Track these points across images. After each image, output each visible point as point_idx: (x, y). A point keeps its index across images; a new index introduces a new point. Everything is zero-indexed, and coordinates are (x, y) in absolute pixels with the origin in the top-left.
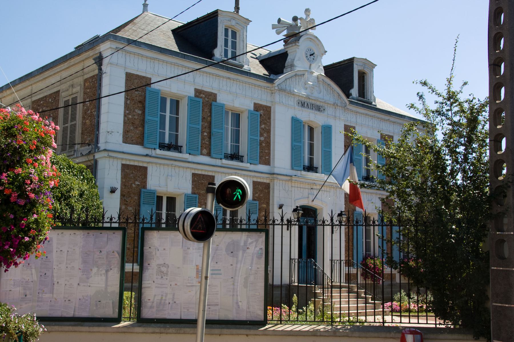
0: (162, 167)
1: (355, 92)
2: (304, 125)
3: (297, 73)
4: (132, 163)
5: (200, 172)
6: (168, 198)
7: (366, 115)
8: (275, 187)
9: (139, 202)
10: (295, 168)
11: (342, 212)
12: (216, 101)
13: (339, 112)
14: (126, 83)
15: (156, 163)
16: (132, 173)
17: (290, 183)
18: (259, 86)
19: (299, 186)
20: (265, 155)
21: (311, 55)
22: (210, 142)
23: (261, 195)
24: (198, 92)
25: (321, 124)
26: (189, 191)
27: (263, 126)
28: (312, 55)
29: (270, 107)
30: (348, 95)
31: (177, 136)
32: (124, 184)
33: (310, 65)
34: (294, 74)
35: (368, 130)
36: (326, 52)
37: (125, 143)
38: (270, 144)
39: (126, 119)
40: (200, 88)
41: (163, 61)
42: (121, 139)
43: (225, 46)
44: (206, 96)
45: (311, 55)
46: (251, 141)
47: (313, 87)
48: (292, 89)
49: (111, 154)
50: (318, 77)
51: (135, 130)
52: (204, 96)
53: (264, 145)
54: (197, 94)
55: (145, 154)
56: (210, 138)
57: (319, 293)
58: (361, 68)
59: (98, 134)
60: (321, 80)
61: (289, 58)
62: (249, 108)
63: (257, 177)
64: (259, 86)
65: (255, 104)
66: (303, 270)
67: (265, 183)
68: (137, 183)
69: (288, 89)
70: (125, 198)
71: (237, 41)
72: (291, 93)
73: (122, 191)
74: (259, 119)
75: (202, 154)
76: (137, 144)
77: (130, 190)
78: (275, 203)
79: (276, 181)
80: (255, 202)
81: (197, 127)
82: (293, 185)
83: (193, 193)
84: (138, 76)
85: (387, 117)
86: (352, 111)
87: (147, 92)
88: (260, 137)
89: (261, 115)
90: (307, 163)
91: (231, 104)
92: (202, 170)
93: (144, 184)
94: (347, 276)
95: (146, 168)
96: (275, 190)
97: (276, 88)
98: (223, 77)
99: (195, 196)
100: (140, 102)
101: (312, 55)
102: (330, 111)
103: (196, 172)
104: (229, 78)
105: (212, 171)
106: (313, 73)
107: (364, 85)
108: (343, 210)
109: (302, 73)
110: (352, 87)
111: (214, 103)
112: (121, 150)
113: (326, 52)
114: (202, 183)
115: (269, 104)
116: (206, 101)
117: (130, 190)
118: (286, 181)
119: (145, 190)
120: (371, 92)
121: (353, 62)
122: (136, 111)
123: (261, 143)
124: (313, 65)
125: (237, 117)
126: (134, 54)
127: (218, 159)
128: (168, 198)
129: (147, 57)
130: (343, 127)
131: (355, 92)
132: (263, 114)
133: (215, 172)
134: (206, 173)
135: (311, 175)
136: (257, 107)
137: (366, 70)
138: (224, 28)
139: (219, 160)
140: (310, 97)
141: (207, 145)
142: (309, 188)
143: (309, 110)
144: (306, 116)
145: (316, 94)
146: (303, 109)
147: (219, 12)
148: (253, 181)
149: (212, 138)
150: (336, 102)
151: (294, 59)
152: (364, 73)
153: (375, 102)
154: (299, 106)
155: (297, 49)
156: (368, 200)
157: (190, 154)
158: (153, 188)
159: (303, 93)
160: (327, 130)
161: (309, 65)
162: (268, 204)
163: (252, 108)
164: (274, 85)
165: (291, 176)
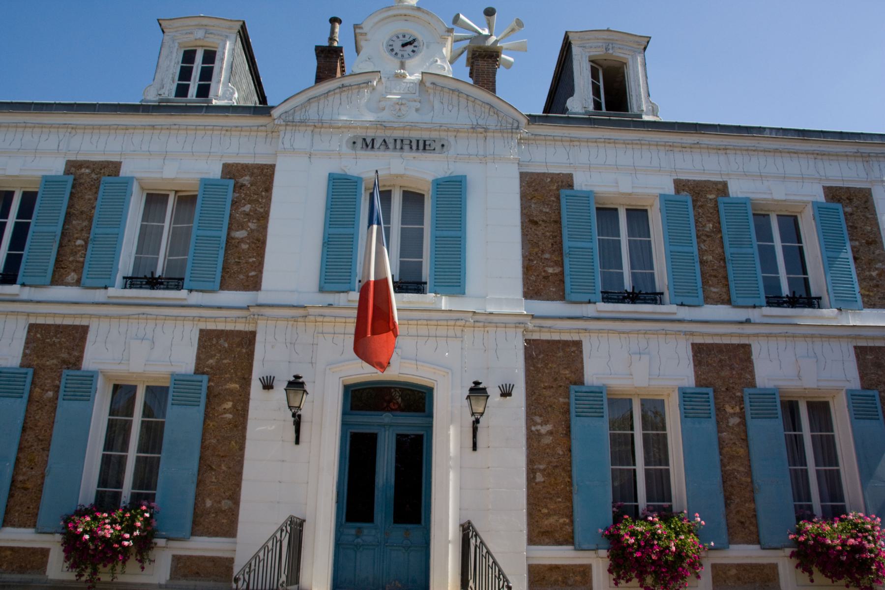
0: (124, 322)
5: (709, 340)
10: (327, 287)
20: (243, 265)
21: (404, 45)
25: (430, 178)
26: (855, 384)
28: (410, 43)
31: (806, 281)
44: (93, 170)
45: (404, 45)
52: (87, 171)
55: (743, 319)
69: (326, 118)
72: (333, 126)
76: (723, 302)
80: (199, 377)
81: (750, 251)
83: (699, 384)
91: (158, 176)
101: (410, 43)
114: (54, 344)
128: (149, 389)
133: (748, 336)
135: (805, 316)
136: (833, 194)
139: (103, 291)
145: (412, 116)
150: (481, 122)
158: (770, 385)
163: (821, 198)
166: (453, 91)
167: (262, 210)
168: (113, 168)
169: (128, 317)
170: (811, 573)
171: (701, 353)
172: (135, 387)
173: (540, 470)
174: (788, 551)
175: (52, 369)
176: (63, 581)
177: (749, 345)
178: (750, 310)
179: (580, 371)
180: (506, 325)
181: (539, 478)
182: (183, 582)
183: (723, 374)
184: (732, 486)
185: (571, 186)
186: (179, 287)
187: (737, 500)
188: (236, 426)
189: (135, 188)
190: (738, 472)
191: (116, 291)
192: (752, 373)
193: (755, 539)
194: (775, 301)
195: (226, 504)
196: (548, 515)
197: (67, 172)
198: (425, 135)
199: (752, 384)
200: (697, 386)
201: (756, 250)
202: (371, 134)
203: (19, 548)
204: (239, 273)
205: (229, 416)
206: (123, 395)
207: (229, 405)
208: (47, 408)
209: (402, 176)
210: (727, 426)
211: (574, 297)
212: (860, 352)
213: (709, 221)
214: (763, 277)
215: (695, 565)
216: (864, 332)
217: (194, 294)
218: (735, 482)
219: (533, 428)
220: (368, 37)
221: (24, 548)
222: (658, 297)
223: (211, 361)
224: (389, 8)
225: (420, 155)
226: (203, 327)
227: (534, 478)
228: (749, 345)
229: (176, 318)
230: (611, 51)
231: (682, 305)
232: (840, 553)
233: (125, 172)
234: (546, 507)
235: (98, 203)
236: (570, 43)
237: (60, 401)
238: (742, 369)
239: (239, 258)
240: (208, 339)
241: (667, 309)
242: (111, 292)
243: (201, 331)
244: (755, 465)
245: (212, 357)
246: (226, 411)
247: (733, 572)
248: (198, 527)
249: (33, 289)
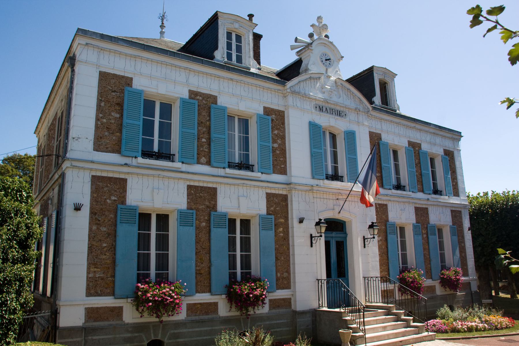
0: (232, 187)
1: (377, 99)
2: (324, 132)
3: (312, 76)
4: (104, 174)
6: (158, 216)
7: (391, 121)
8: (294, 199)
9: (116, 221)
11: (373, 223)
12: (216, 103)
13: (362, 118)
14: (99, 83)
15: (138, 174)
16: (107, 186)
17: (311, 194)
18: (268, 89)
19: (322, 197)
20: (279, 163)
21: (326, 60)
22: (209, 149)
23: (277, 209)
24: (193, 94)
25: (343, 130)
27: (276, 132)
29: (283, 112)
30: (372, 103)
32: (95, 200)
33: (327, 69)
34: (309, 76)
35: (395, 137)
36: (342, 57)
37: (97, 151)
38: (285, 151)
39: (99, 123)
40: (195, 89)
41: (147, 59)
42: (90, 145)
43: (227, 49)
44: (203, 99)
45: (326, 60)
46: (261, 148)
47: (331, 91)
48: (307, 93)
49: (74, 163)
50: (336, 82)
51: (109, 137)
52: (200, 98)
53: (278, 152)
54: (193, 96)
55: (124, 163)
56: (209, 145)
57: (349, 320)
58: (381, 77)
59: (67, 143)
60: (339, 84)
61: (303, 64)
62: (258, 112)
63: (271, 188)
64: (268, 89)
65: (265, 108)
66: (333, 290)
67: (281, 195)
68: (113, 198)
70: (97, 216)
71: (243, 45)
72: (305, 96)
73: (91, 208)
74: (270, 125)
75: (199, 163)
76: (113, 152)
77: (104, 207)
78: (294, 217)
79: (293, 192)
82: (315, 196)
84: (115, 76)
85: (413, 125)
86: (376, 118)
87: (126, 93)
88: (273, 143)
89: (272, 120)
90: (330, 172)
92: (199, 181)
93: (122, 199)
94: (383, 293)
95: (125, 181)
96: (293, 202)
97: (289, 90)
98: (224, 78)
99: (191, 211)
100: (118, 104)
102: (352, 116)
103: (192, 184)
104: (232, 79)
105: (212, 182)
106: (330, 77)
107: (386, 95)
108: (375, 221)
109: (317, 76)
110: (374, 95)
111: (213, 106)
112: (90, 159)
113: (342, 57)
114: (201, 197)
115: (281, 109)
116: (203, 105)
117: (104, 207)
118: (306, 191)
119: (122, 206)
120: (394, 100)
121: (373, 71)
122: (113, 114)
123: (274, 150)
124: (330, 70)
125: (245, 123)
126: (110, 51)
127: (221, 168)
128: (158, 216)
129: (126, 55)
130: (368, 139)
131: (377, 99)
132: (276, 120)
133: (216, 183)
134: (205, 185)
136: (268, 111)
137: (387, 80)
138: (225, 31)
139: (222, 170)
140: (329, 101)
141: (206, 153)
142: (334, 198)
143: (328, 115)
144: (325, 121)
145: (335, 99)
146: (321, 113)
147: (219, 14)
148: (267, 193)
149: (212, 144)
150: (358, 107)
151: (308, 64)
152: (385, 83)
153: (399, 110)
154: (316, 110)
155: (311, 54)
156: (401, 210)
157: (183, 163)
158: (134, 204)
159: (320, 96)
160: (350, 136)
161: (325, 70)
162: (286, 218)
164: (286, 88)
165: (312, 186)
166: (348, 89)
167: (282, 134)
169: (238, 185)
170: (231, 304)
171: (269, 196)
174: (439, 281)
175: (202, 210)
176: (228, 317)
177: (126, 179)
179: (387, 216)
182: (274, 311)
185: (216, 103)
188: (285, 239)
194: (147, 154)
195: (285, 275)
200: (267, 214)
201: (141, 123)
202: (321, 104)
203: (204, 303)
204: (277, 165)
205: (282, 234)
207: (281, 229)
208: (204, 231)
209: (333, 127)
212: (452, 211)
214: (143, 138)
215: (179, 305)
216: (454, 205)
220: (313, 51)
221: (206, 303)
222: (171, 157)
223: (272, 208)
226: (94, 174)
228: (126, 179)
229: (258, 187)
236: (218, 18)
237: (212, 229)
239: (276, 158)
241: (256, 175)
244: (431, 251)
245: (272, 206)
246: (280, 232)
248: (280, 287)
249: (187, 165)
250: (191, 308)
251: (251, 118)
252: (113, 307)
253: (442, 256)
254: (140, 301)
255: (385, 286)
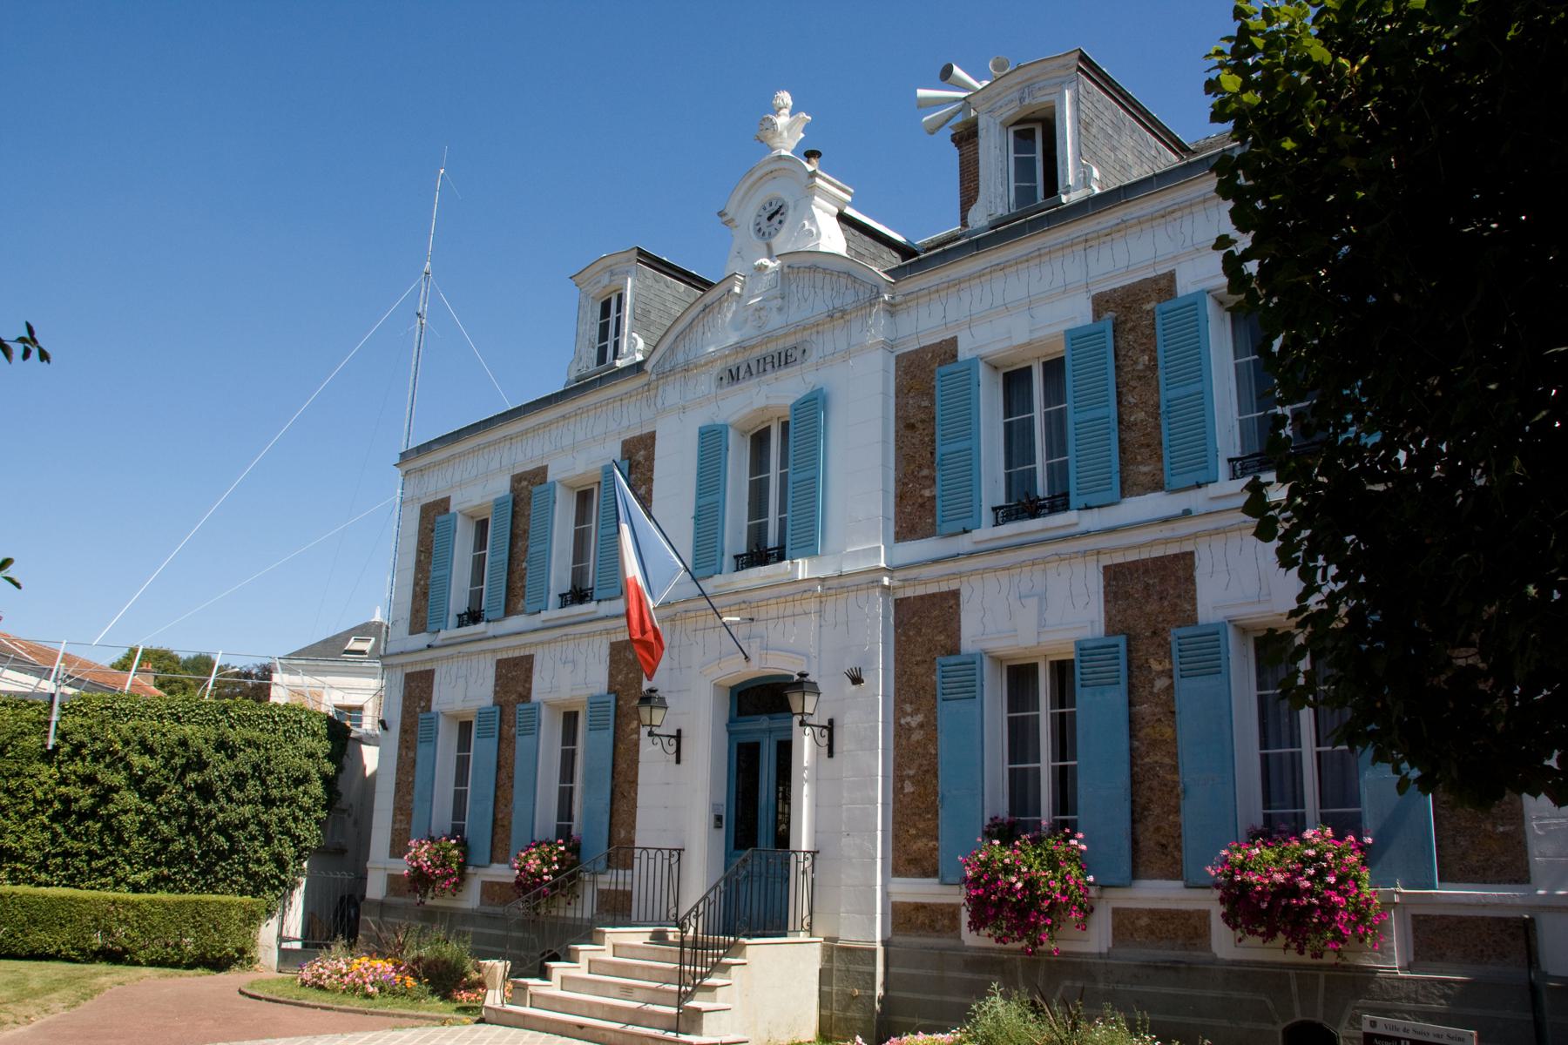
18: (629, 394)
21: (770, 219)
45: (770, 219)
55: (1179, 511)
76: (1154, 490)
145: (775, 321)
168: (947, 351)
169: (555, 640)
172: (1035, 665)
173: (909, 777)
178: (1192, 493)
179: (955, 635)
180: (858, 588)
181: (909, 788)
183: (1148, 609)
184: (1151, 788)
186: (1065, 507)
187: (1157, 811)
189: (983, 372)
190: (1161, 765)
191: (986, 533)
192: (1193, 600)
193: (1174, 871)
196: (916, 837)
197: (1097, 315)
198: (780, 345)
199: (1192, 620)
202: (731, 362)
206: (1020, 677)
210: (1151, 693)
211: (1177, 481)
213: (1143, 351)
217: (603, 604)
218: (1155, 783)
219: (903, 721)
224: (751, 172)
225: (784, 372)
227: (902, 788)
229: (589, 634)
230: (1027, 101)
231: (1088, 508)
232: (1262, 894)
233: (964, 353)
234: (915, 826)
235: (938, 408)
238: (1179, 596)
240: (1116, 577)
242: (977, 535)
243: (612, 644)
245: (620, 672)
247: (1144, 921)
250: (1124, 922)
251: (572, 488)
252: (1169, 911)
253: (566, 797)
254: (1244, 905)
255: (621, 879)
